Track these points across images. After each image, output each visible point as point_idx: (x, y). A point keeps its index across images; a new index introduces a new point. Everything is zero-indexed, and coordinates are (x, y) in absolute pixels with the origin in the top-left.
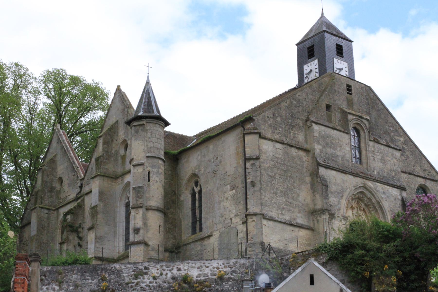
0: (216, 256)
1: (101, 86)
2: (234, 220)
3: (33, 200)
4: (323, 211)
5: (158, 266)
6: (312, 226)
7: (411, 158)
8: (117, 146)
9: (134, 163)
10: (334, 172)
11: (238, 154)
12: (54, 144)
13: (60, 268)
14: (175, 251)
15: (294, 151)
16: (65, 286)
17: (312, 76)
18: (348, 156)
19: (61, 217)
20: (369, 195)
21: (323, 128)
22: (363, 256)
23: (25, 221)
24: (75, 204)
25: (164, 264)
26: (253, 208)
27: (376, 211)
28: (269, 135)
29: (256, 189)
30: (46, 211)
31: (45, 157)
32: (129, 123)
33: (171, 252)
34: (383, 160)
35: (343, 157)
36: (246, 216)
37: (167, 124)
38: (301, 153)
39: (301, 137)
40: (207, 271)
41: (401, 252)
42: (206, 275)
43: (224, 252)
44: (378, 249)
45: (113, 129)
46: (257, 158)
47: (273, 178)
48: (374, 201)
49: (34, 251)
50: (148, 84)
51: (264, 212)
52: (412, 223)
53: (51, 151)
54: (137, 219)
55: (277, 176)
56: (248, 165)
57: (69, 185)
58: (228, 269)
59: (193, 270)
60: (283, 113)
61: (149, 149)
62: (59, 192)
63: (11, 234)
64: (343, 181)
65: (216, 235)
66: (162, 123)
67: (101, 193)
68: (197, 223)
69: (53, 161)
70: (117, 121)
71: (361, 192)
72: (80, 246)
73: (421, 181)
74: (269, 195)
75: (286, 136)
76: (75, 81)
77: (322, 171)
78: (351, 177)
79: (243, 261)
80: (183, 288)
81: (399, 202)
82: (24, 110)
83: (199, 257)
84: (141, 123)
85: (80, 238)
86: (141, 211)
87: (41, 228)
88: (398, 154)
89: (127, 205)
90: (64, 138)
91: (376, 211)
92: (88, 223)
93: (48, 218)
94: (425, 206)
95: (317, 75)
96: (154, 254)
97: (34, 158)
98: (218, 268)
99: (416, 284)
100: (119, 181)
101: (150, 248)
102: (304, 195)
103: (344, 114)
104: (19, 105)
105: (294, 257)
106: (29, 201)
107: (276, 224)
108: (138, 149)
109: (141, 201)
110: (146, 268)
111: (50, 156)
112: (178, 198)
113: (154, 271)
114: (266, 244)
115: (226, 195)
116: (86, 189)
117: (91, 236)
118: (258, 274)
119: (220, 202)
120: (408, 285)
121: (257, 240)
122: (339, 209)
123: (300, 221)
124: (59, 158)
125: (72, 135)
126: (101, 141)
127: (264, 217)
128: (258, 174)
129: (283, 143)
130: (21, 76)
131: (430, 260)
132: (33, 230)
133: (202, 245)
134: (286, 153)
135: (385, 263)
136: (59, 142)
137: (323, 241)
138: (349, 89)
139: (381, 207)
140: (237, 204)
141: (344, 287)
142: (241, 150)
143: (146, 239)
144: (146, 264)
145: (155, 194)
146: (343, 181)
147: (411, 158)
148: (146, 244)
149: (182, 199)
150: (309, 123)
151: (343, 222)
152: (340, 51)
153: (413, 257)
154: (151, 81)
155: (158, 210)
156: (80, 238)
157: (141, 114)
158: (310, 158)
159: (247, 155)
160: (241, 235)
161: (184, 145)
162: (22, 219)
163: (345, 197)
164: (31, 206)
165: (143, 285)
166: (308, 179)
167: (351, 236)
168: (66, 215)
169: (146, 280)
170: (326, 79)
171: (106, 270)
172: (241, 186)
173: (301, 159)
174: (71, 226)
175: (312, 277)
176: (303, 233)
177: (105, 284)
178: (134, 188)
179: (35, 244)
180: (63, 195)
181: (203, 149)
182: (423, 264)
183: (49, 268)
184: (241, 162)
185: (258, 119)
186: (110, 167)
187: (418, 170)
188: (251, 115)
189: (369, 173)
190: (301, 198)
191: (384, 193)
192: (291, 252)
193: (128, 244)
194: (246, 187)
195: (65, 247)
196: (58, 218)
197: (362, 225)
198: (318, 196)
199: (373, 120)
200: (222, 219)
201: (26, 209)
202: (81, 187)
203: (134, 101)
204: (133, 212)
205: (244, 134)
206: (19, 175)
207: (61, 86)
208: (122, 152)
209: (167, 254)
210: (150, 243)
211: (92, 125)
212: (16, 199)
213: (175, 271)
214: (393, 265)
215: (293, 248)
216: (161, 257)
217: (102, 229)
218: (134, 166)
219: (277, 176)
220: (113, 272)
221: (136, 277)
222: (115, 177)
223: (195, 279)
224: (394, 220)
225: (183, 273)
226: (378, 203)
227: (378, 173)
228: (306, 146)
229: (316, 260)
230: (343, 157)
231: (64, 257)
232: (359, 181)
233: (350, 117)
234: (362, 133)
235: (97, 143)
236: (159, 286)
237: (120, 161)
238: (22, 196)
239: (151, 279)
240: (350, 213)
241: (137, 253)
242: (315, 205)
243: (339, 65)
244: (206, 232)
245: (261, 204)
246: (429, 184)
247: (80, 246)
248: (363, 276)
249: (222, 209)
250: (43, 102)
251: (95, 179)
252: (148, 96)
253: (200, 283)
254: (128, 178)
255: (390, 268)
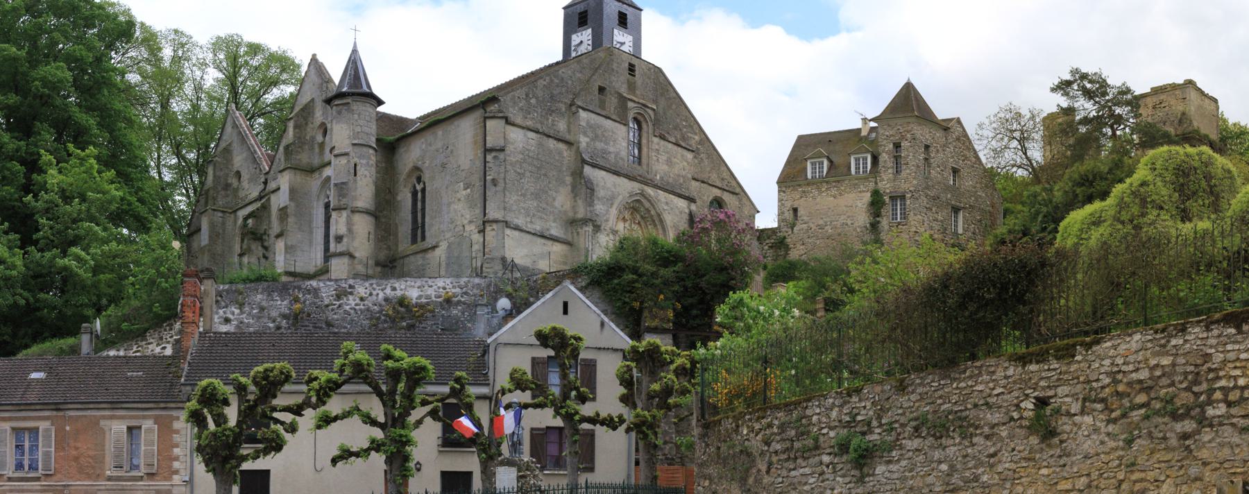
0: (443, 273)
1: (289, 54)
2: (468, 228)
3: (202, 201)
4: (585, 221)
5: (367, 284)
6: (570, 239)
7: (706, 162)
8: (312, 132)
9: (336, 152)
10: (603, 173)
11: (475, 143)
12: (229, 128)
13: (241, 286)
14: (389, 266)
15: (552, 143)
16: (247, 309)
17: (583, 49)
18: (624, 153)
19: (240, 221)
20: (647, 205)
21: (593, 116)
22: (634, 281)
23: (192, 229)
24: (258, 204)
25: (374, 281)
26: (493, 213)
27: (655, 225)
28: (519, 121)
29: (498, 188)
30: (220, 214)
31: (217, 146)
32: (328, 101)
33: (384, 266)
34: (669, 162)
35: (617, 154)
36: (484, 223)
37: (380, 102)
38: (561, 146)
39: (562, 126)
40: (431, 292)
41: (683, 280)
42: (428, 297)
43: (454, 268)
44: (652, 274)
45: (308, 110)
46: (502, 150)
47: (522, 175)
48: (653, 212)
49: (206, 265)
50: (355, 51)
51: (508, 219)
52: (698, 244)
53: (224, 138)
54: (339, 224)
55: (528, 174)
56: (489, 158)
57: (250, 180)
58: (458, 290)
59: (413, 290)
60: (540, 93)
61: (356, 135)
62: (237, 190)
63: (176, 245)
64: (615, 186)
65: (444, 246)
66: (374, 102)
67: (293, 191)
68: (418, 230)
69: (227, 151)
70: (313, 100)
71: (638, 201)
72: (265, 257)
73: (717, 192)
74: (516, 198)
75: (542, 123)
76: (255, 49)
77: (588, 170)
78: (626, 181)
79: (477, 280)
80: (398, 312)
81: (686, 217)
82: (188, 89)
83: (421, 274)
84: (344, 101)
85: (266, 248)
86: (344, 214)
87: (215, 235)
88: (690, 156)
89: (327, 206)
90: (243, 123)
91: (655, 225)
92: (276, 228)
93: (223, 224)
94: (719, 224)
95: (590, 48)
96: (360, 269)
97: (203, 148)
98: (444, 288)
99: (698, 321)
100: (316, 175)
101: (356, 261)
102: (562, 199)
103: (623, 100)
104: (179, 81)
105: (544, 278)
106: (198, 201)
107: (523, 234)
108: (341, 135)
109: (344, 201)
110: (351, 287)
111: (223, 145)
112: (394, 198)
113: (361, 290)
114: (509, 260)
115: (458, 195)
116: (272, 185)
117: (280, 245)
118: (496, 300)
119: (449, 204)
120: (687, 322)
121: (497, 254)
122: (607, 221)
123: (554, 232)
124: (236, 147)
125: (251, 117)
126: (291, 124)
127: (507, 224)
128: (502, 169)
129: (537, 132)
130: (181, 42)
131: (718, 292)
132: (204, 238)
133: (424, 259)
134: (540, 145)
135: (661, 292)
136: (235, 126)
137: (583, 259)
138: (632, 68)
139: (661, 221)
140: (472, 207)
141: (606, 319)
142: (480, 138)
143: (352, 250)
144: (351, 282)
145: (364, 192)
146: (615, 186)
147: (706, 162)
148: (352, 256)
149: (399, 198)
150: (574, 109)
151: (611, 237)
152: (623, 20)
153: (697, 287)
154: (359, 49)
155: (367, 212)
156: (266, 248)
157: (345, 89)
158: (573, 153)
159: (489, 145)
160: (475, 247)
161: (403, 130)
162: (189, 225)
163: (615, 206)
164: (201, 208)
165: (347, 308)
166: (569, 179)
167: (620, 255)
168: (246, 219)
169: (352, 301)
170: (602, 55)
171: (299, 288)
172: (479, 185)
173: (560, 153)
174: (253, 233)
175: (566, 305)
176: (557, 248)
177: (298, 306)
178: (336, 185)
179: (206, 257)
180: (241, 194)
181: (428, 136)
182: (708, 297)
183: (227, 287)
184: (481, 155)
185: (505, 99)
186: (304, 158)
187: (714, 178)
188: (496, 94)
189: (649, 177)
190: (557, 204)
191: (667, 203)
192: (541, 272)
193: (328, 256)
194: (485, 186)
195: (245, 259)
196: (235, 221)
197: (636, 243)
198: (580, 202)
199: (661, 111)
200: (452, 226)
201: (194, 212)
202: (265, 183)
203: (336, 72)
204: (334, 215)
205: (485, 118)
206: (183, 170)
207: (234, 55)
208: (319, 138)
209: (379, 269)
210: (357, 255)
211: (280, 103)
212: (180, 201)
213: (388, 291)
214: (670, 295)
215: (544, 266)
216: (370, 272)
217: (294, 237)
218: (336, 156)
219: (528, 174)
220: (309, 292)
221: (338, 297)
222: (311, 170)
223: (414, 301)
224: (678, 239)
225: (399, 293)
226: (659, 215)
227: (662, 178)
228: (568, 137)
229: (573, 283)
230: (617, 154)
231: (245, 272)
232: (636, 187)
233: (630, 104)
234: (644, 126)
235: (286, 127)
236: (368, 310)
237: (317, 150)
238: (188, 197)
239: (358, 301)
240: (620, 226)
241: (339, 267)
242: (575, 213)
243: (621, 38)
244: (430, 241)
245: (505, 209)
246: (726, 197)
247: (265, 257)
248: (632, 309)
249: (452, 213)
250: (212, 77)
251: (284, 173)
252: (354, 67)
253: (421, 306)
254: (328, 172)
255: (666, 299)
